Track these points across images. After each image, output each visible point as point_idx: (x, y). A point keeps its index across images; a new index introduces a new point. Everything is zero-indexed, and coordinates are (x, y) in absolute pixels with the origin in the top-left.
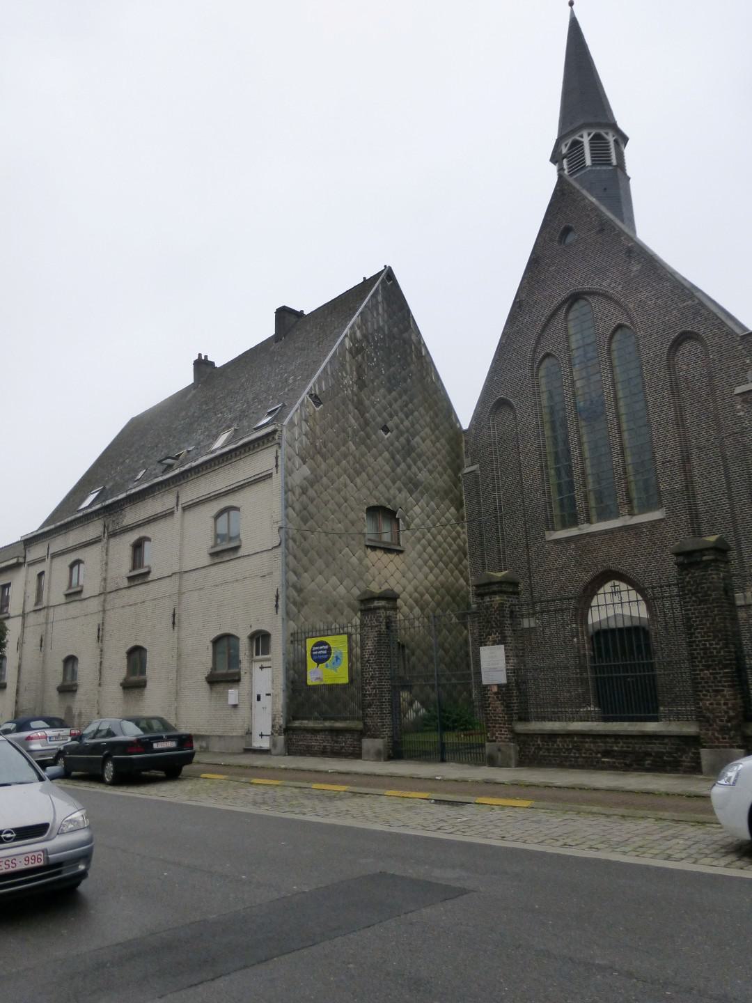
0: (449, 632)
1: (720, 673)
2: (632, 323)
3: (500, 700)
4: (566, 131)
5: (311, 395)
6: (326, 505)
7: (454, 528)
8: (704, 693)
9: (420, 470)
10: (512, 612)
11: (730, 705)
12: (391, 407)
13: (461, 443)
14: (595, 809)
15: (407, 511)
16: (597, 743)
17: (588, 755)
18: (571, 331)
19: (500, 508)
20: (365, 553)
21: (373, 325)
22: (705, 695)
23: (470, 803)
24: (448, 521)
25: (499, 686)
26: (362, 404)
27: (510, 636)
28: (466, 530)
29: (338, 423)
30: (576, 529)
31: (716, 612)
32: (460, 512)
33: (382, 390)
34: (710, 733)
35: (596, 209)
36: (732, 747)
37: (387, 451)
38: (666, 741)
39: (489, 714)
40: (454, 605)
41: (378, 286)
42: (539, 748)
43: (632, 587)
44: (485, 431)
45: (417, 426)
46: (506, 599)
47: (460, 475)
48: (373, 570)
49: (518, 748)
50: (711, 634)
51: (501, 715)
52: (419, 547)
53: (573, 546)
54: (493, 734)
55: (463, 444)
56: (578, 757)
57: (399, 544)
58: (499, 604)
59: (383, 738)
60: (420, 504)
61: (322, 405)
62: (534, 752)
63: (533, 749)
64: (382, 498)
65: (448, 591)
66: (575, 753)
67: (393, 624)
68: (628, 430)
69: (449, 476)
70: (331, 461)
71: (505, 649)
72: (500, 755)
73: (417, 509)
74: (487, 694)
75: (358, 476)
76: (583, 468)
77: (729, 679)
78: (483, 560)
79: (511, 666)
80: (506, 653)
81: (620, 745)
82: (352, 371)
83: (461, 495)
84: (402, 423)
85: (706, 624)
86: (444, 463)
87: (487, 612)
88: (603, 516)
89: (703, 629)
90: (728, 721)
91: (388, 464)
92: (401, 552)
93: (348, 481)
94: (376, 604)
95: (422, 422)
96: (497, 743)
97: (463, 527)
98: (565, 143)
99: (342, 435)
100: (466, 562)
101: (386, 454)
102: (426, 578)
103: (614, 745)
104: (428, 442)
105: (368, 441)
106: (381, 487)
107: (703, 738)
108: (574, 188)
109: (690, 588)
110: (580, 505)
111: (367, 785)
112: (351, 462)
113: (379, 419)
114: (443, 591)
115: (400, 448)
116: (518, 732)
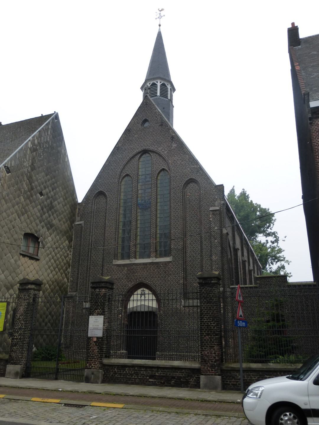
0: (55, 306)
1: (214, 338)
2: (169, 169)
3: (97, 346)
4: (152, 77)
5: (5, 167)
6: (2, 228)
7: (66, 251)
8: (205, 347)
9: (55, 219)
10: (109, 298)
11: (217, 354)
12: (46, 183)
13: (77, 209)
14: (161, 409)
15: (44, 239)
16: (148, 371)
17: (142, 377)
18: (140, 167)
19: (91, 245)
20: (19, 258)
21: (44, 139)
22: (205, 348)
23: (87, 406)
24: (64, 247)
25: (98, 338)
26: (31, 178)
27: (107, 311)
28: (72, 253)
29: (17, 185)
30: (128, 260)
31: (215, 308)
32: (70, 244)
33: (43, 174)
34: (206, 367)
35: (161, 115)
36: (216, 375)
37: (40, 205)
38: (183, 371)
39: (89, 353)
40: (60, 291)
41: (50, 121)
42: (115, 373)
43: (151, 292)
44: (90, 205)
45: (57, 196)
46: (107, 291)
47: (73, 225)
48: (22, 268)
49: (103, 373)
50: (211, 318)
51: (97, 354)
52: (47, 259)
53: (126, 269)
54: (90, 365)
55: (77, 210)
56: (136, 379)
57: (37, 255)
58: (104, 293)
59: (21, 365)
60: (51, 236)
61: (10, 173)
62: (112, 375)
63: (112, 373)
64: (33, 230)
65: (58, 284)
66: (135, 376)
67: (37, 299)
68: (159, 218)
69: (68, 224)
70: (10, 204)
71: (104, 318)
72: (93, 376)
73: (50, 238)
74: (90, 342)
75: (23, 216)
76: (136, 232)
77: (217, 341)
78: (78, 269)
79: (106, 327)
80: (104, 320)
81: (159, 372)
82: (29, 159)
83: (72, 235)
84: (50, 193)
85: (209, 313)
86: (67, 217)
87: (96, 297)
88: (142, 257)
89: (208, 315)
90: (215, 362)
91: (39, 212)
92: (38, 260)
93: (17, 217)
94: (30, 286)
95: (59, 194)
96: (92, 370)
97: (70, 252)
98: (150, 83)
99: (18, 192)
100: (69, 270)
101: (39, 207)
102: (48, 276)
103: (157, 372)
104: (61, 205)
105: (31, 198)
106: (34, 224)
107: (202, 370)
108: (152, 103)
109: (204, 295)
110: (133, 249)
111: (22, 395)
112: (20, 208)
113: (39, 188)
114: (55, 283)
115: (47, 205)
116: (104, 364)
